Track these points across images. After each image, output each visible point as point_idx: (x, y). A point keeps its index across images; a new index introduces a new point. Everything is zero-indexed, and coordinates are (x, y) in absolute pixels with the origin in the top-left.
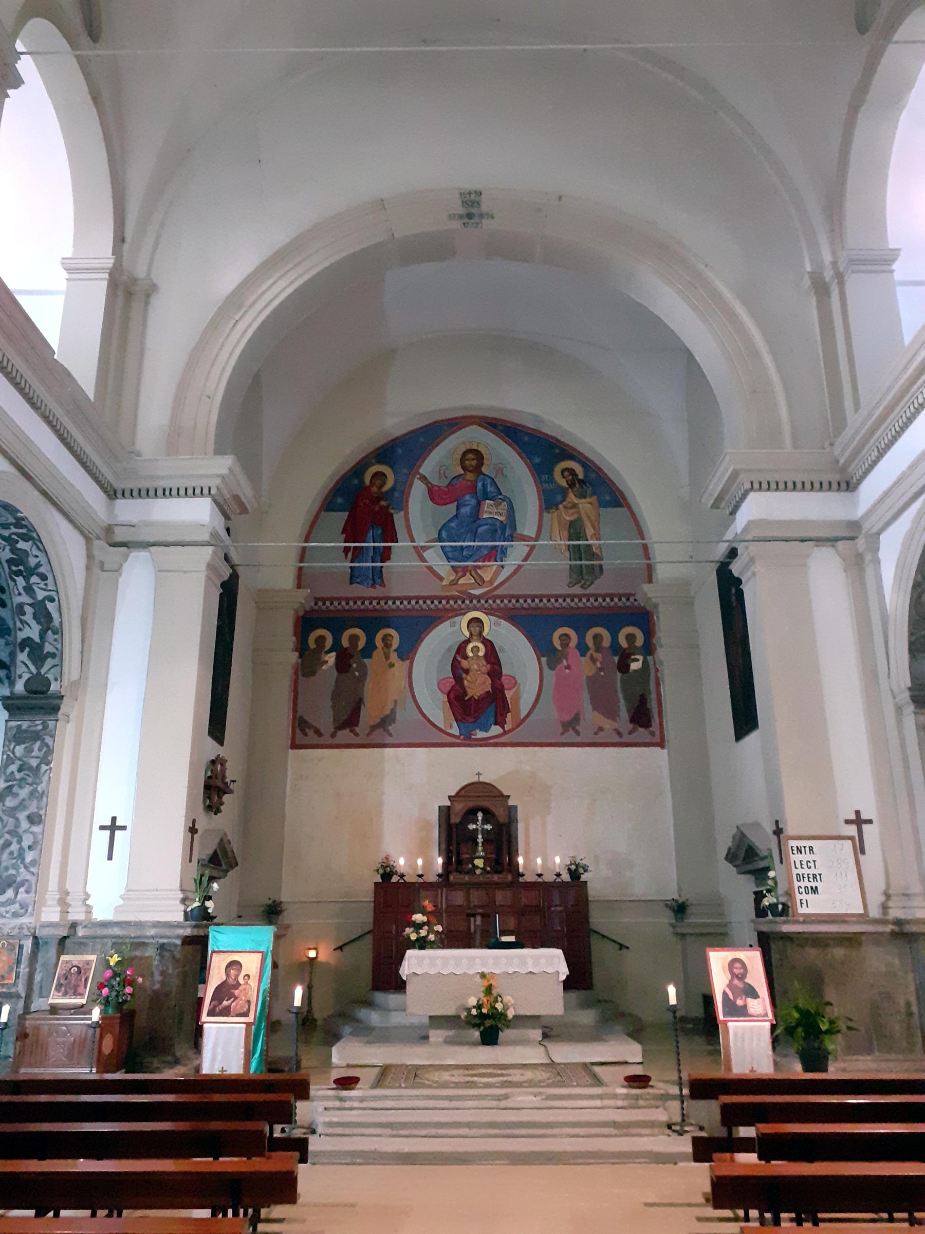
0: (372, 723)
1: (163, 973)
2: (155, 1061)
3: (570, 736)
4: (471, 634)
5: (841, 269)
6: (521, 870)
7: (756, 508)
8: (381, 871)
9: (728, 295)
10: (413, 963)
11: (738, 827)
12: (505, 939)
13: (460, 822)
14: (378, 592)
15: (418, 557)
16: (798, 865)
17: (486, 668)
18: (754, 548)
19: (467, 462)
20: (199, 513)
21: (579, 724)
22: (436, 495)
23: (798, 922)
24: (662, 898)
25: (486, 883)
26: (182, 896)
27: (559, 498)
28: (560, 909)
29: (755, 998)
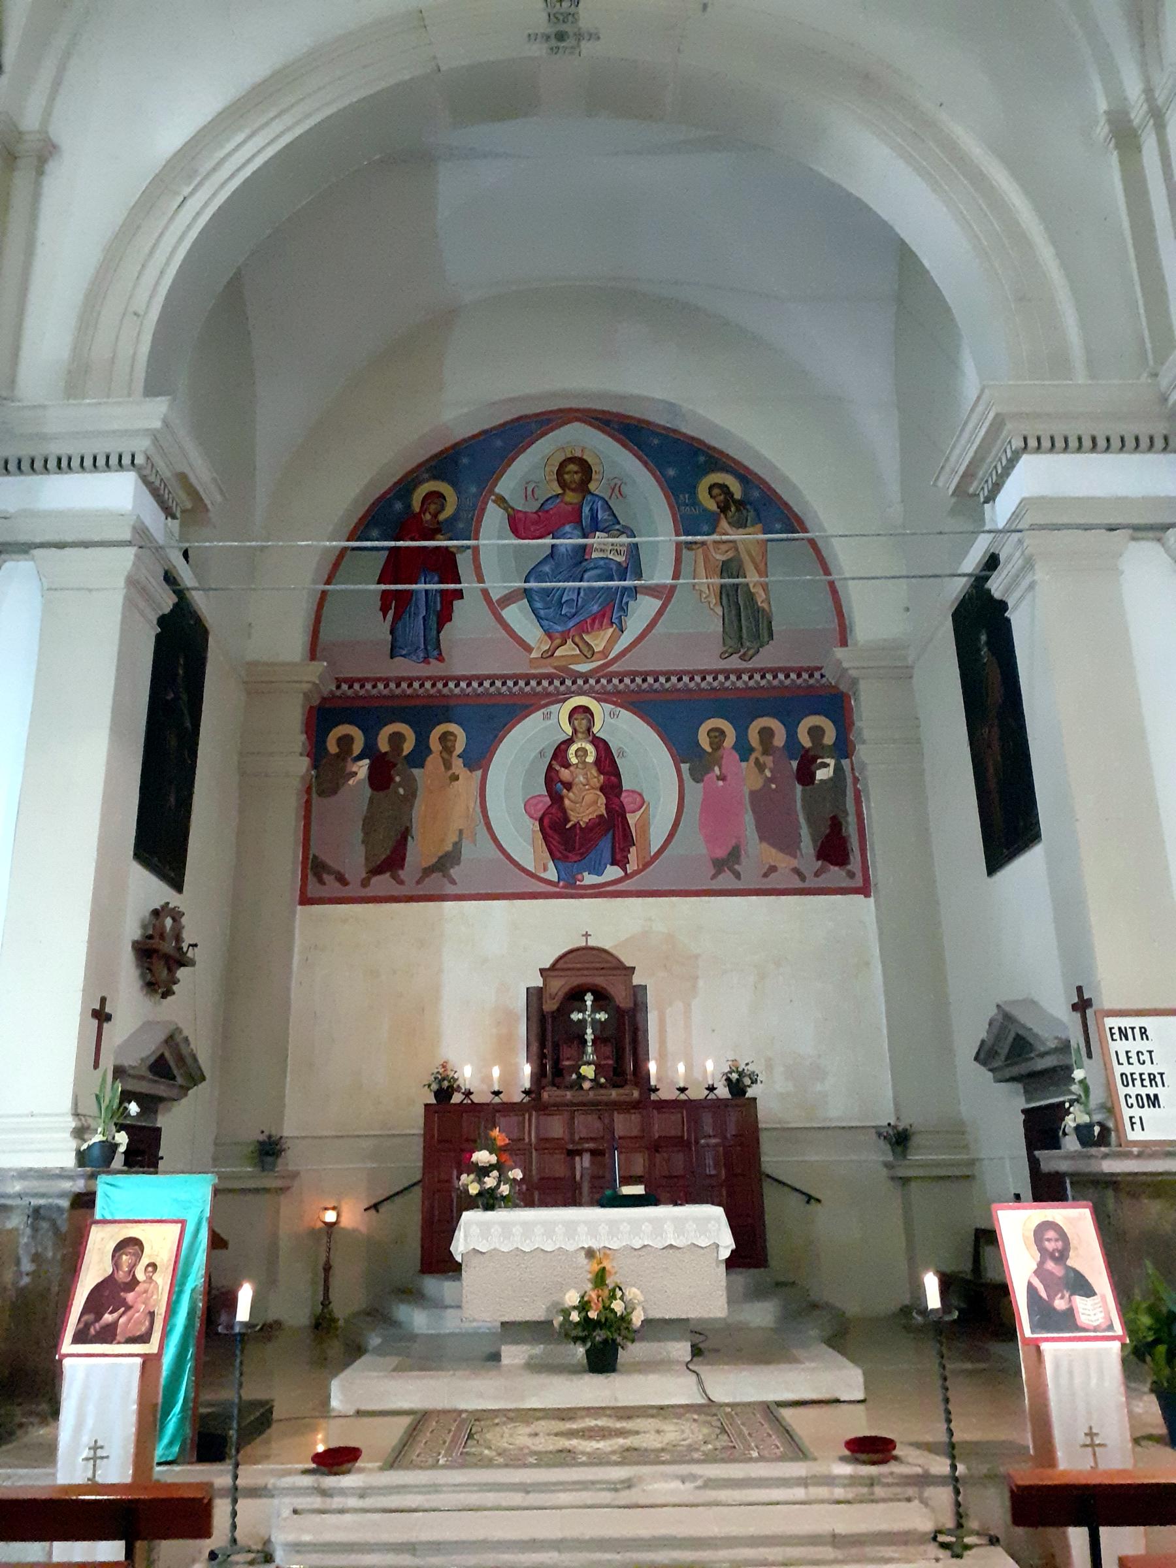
0: (425, 865)
1: (36, 1258)
2: (18, 1411)
3: (726, 880)
4: (575, 731)
5: (1160, 102)
6: (653, 1082)
7: (1032, 478)
8: (435, 1087)
9: (976, 150)
10: (474, 1232)
11: (998, 1006)
12: (627, 1190)
13: (558, 1010)
14: (434, 668)
15: (494, 620)
16: (1123, 1059)
17: (598, 780)
18: (1032, 541)
19: (566, 476)
20: (117, 495)
21: (738, 863)
22: (518, 525)
23: (1127, 1155)
24: (873, 1124)
25: (599, 1103)
26: (73, 1125)
28: (713, 1141)
29: (1088, 1296)
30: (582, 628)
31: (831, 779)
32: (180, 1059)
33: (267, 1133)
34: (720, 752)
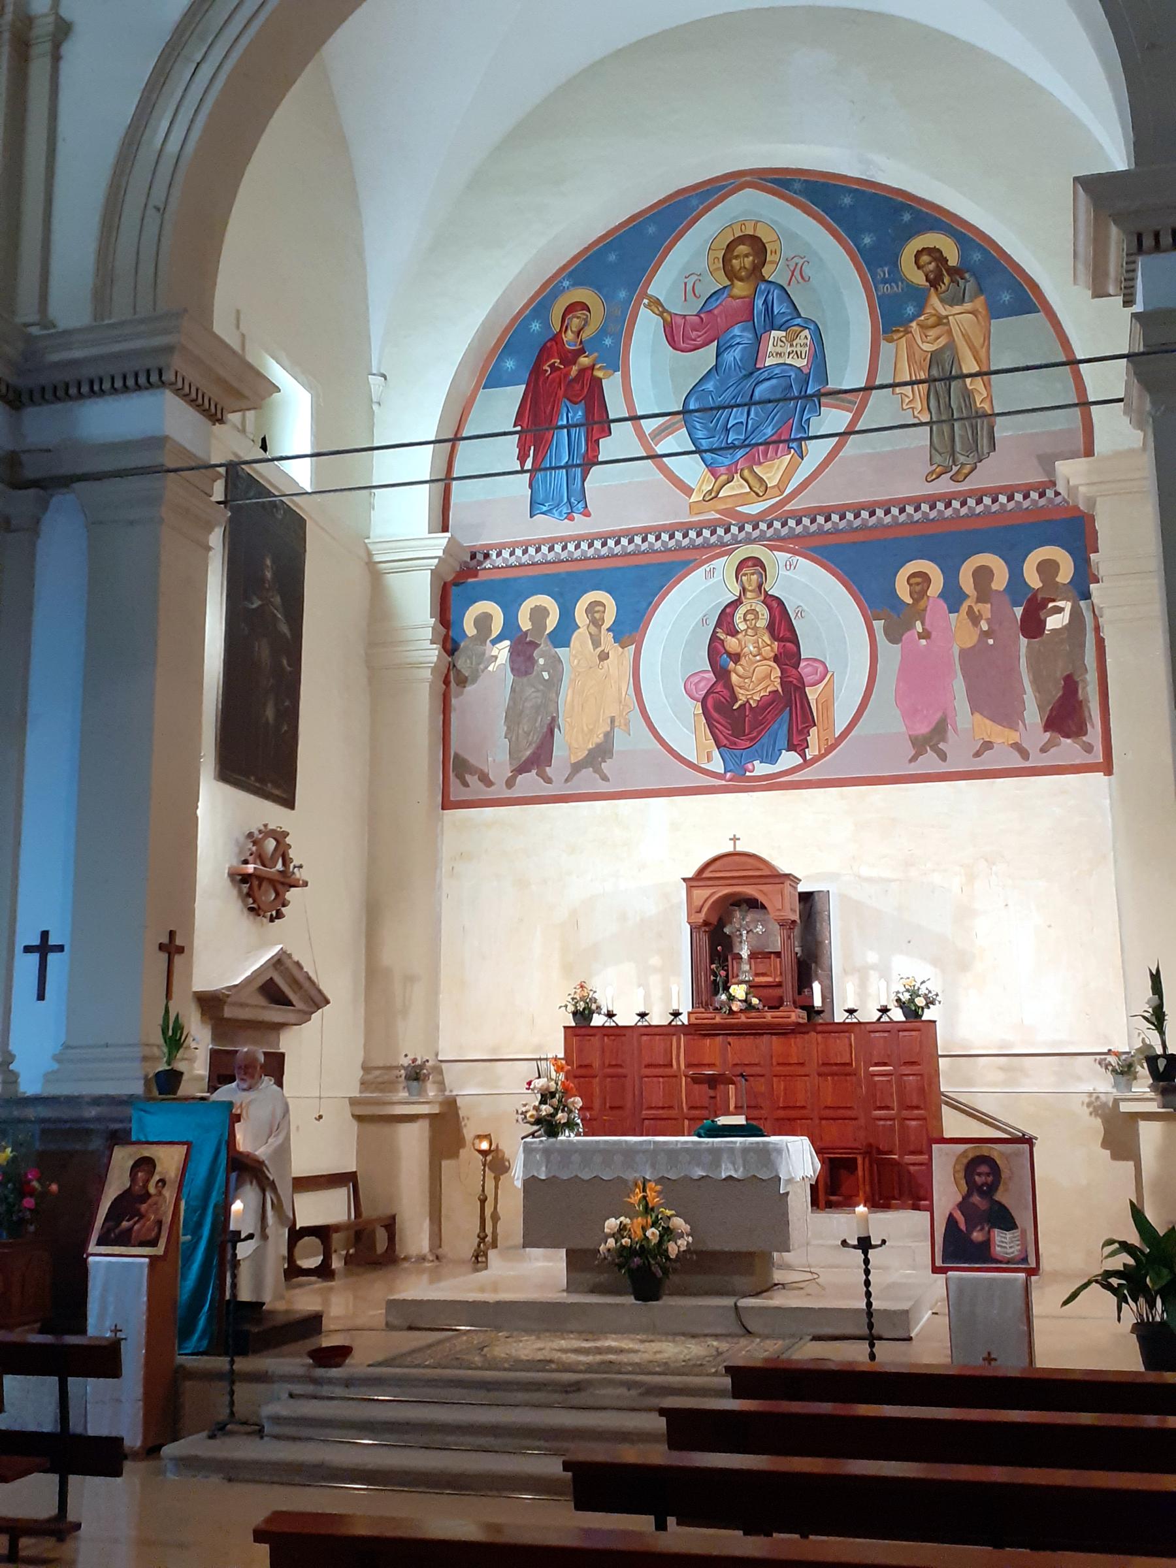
3: (929, 762)
4: (744, 590)
8: (571, 1008)
17: (770, 648)
21: (944, 740)
22: (677, 335)
27: (910, 310)
30: (753, 461)
31: (1065, 628)
32: (295, 983)
33: (411, 1057)
34: (922, 604)
